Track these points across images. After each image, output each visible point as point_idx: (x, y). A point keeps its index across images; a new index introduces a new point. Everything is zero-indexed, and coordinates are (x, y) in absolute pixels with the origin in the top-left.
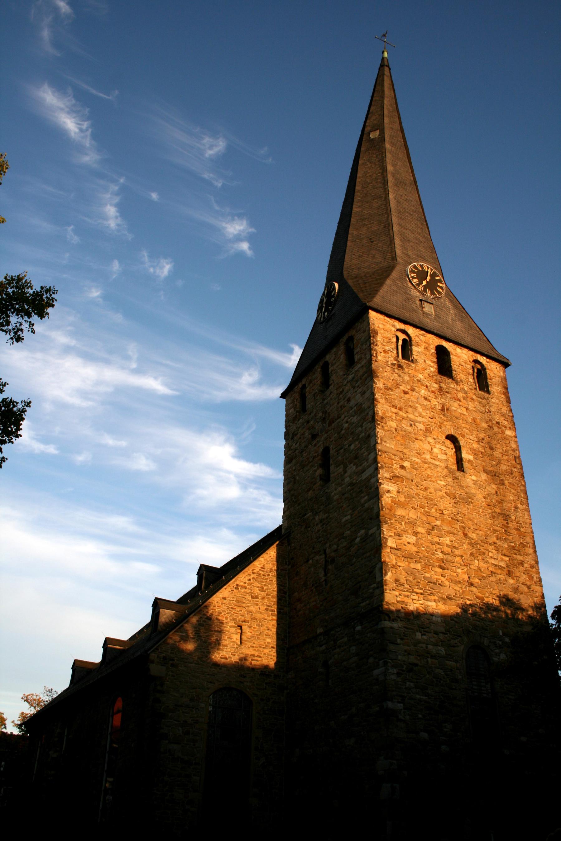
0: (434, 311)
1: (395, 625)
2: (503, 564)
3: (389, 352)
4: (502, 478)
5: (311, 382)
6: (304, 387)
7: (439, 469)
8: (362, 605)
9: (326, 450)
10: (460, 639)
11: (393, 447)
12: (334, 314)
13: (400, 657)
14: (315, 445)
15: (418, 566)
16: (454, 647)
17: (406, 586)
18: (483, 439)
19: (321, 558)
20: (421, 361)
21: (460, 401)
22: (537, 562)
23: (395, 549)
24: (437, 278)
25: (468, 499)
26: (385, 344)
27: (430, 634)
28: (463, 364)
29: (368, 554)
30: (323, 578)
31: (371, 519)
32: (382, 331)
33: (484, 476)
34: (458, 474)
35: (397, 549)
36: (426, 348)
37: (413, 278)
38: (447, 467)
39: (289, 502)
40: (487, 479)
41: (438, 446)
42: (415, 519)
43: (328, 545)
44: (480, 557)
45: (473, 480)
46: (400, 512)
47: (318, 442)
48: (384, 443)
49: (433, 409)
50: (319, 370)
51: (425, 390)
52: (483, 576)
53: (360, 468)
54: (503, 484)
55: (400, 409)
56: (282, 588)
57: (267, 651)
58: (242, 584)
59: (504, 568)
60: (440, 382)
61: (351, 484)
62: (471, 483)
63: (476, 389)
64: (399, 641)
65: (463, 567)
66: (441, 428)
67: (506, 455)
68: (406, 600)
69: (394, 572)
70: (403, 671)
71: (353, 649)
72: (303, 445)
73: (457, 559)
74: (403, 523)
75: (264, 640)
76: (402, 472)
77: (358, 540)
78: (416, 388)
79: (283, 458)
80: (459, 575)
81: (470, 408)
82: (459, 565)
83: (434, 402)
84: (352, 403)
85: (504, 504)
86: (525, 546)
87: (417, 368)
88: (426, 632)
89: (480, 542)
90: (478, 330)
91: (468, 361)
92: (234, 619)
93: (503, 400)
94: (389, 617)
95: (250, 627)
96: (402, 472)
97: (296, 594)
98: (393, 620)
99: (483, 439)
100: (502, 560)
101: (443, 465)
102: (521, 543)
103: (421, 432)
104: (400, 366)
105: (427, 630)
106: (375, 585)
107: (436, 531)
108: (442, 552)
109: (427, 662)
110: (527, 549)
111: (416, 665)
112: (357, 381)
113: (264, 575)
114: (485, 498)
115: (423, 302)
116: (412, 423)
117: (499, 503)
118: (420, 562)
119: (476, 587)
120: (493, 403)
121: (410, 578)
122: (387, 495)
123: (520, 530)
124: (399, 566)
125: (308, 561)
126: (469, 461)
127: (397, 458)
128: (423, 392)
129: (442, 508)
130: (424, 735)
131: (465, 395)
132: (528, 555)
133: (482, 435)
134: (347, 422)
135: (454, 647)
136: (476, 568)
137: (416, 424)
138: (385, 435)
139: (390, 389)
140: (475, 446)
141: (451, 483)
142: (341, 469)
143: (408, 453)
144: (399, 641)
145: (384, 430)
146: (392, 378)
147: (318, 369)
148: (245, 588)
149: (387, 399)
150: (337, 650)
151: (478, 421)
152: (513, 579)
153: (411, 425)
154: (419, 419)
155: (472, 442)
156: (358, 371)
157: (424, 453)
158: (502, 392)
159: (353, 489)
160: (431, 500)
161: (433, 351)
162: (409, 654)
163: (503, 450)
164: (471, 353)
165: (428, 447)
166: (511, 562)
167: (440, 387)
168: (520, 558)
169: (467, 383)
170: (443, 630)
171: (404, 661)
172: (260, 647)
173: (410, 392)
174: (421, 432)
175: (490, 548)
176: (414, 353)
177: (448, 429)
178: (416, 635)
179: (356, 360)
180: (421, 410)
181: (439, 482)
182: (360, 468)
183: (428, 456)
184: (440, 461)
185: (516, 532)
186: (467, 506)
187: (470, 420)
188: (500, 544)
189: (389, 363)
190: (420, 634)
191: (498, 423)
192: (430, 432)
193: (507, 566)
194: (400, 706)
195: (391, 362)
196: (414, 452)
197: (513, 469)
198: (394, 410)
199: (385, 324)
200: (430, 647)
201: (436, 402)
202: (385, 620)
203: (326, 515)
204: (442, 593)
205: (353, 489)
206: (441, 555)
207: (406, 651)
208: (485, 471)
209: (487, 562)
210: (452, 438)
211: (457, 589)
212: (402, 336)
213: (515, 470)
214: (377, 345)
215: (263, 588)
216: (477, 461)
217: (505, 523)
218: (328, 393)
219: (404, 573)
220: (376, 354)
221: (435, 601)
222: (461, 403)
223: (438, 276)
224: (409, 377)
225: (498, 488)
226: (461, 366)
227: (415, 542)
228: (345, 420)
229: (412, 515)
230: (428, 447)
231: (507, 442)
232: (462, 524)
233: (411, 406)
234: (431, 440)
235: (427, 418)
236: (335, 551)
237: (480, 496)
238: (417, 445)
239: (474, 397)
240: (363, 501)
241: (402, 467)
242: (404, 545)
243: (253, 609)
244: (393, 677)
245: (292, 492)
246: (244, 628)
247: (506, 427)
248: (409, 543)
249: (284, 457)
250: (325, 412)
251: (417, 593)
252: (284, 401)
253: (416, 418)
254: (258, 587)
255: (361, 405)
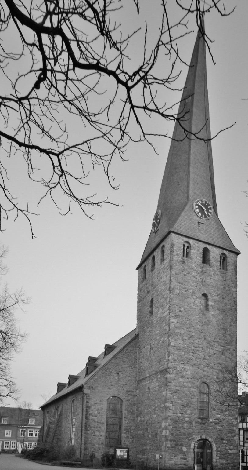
0: (205, 228)
1: (171, 376)
2: (220, 350)
3: (179, 255)
4: (226, 312)
5: (148, 264)
6: (145, 266)
7: (197, 311)
8: (161, 367)
9: (152, 300)
10: (197, 380)
11: (177, 302)
12: (158, 230)
13: (172, 388)
14: (149, 297)
15: (183, 353)
16: (195, 383)
17: (177, 361)
18: (220, 294)
19: (149, 347)
20: (194, 258)
21: (211, 276)
22: (236, 348)
23: (174, 346)
24: (209, 207)
25: (209, 323)
26: (178, 251)
27: (185, 379)
28: (216, 256)
29: (164, 348)
30: (149, 355)
31: (166, 334)
32: (177, 244)
33: (218, 312)
34: (205, 312)
35: (175, 346)
36: (198, 250)
37: (196, 209)
38: (200, 310)
39: (139, 321)
40: (219, 313)
41: (198, 300)
42: (184, 334)
43: (151, 342)
44: (211, 348)
45: (212, 314)
46: (177, 331)
47: (149, 295)
48: (173, 301)
49: (197, 282)
50: (151, 259)
51: (195, 272)
52: (211, 356)
53: (163, 311)
54: (226, 315)
55: (182, 284)
56: (135, 357)
57: (129, 382)
58: (119, 357)
59: (221, 351)
60: (202, 268)
61: (160, 317)
62: (211, 316)
63: (221, 268)
64: (172, 382)
65: (202, 352)
66: (200, 291)
67: (230, 301)
68: (177, 366)
69: (172, 355)
70: (173, 392)
71: (157, 384)
72: (144, 295)
73: (200, 349)
74: (178, 336)
75: (128, 378)
76: (180, 313)
77: (161, 342)
78: (190, 272)
79: (137, 300)
80: (200, 355)
81: (216, 279)
82: (201, 351)
83: (199, 278)
84: (162, 280)
85: (225, 324)
86: (232, 342)
87: (192, 261)
88: (184, 378)
89: (211, 341)
90: (227, 236)
91: (218, 254)
92: (116, 371)
93: (233, 273)
94: (169, 373)
95: (122, 374)
96: (180, 313)
97: (140, 360)
98: (171, 374)
99: (220, 294)
100: (220, 348)
101: (199, 308)
102: (230, 341)
103: (190, 294)
104: (184, 262)
105: (184, 377)
106: (165, 361)
107: (192, 338)
108: (194, 346)
109: (183, 389)
110: (232, 343)
111: (179, 390)
112: (165, 269)
113: (128, 353)
114: (216, 322)
115: (199, 223)
116: (187, 290)
117: (223, 323)
118: (184, 351)
119: (207, 360)
120: (228, 275)
121: (179, 358)
122: (172, 324)
123: (231, 335)
124: (175, 353)
125: (144, 347)
126: (212, 306)
127: (178, 307)
128: (193, 274)
129: (196, 328)
130: (180, 415)
131: (214, 273)
132: (232, 345)
133: (219, 292)
134: (160, 289)
135: (195, 383)
136: (208, 352)
137: (189, 290)
138: (173, 297)
139: (178, 274)
140: (216, 298)
141: (201, 316)
142: (157, 310)
143: (183, 305)
144: (172, 382)
145: (173, 295)
146: (179, 269)
147: (151, 258)
148: (120, 358)
149: (176, 279)
150: (152, 384)
151: (219, 285)
152: (224, 356)
153: (186, 291)
154: (191, 287)
155: (214, 296)
156: (165, 264)
157: (191, 304)
158: (234, 269)
159: (160, 320)
160: (191, 325)
161: (202, 251)
162: (176, 386)
163: (229, 298)
164: (221, 249)
165: (193, 300)
166: (224, 349)
167: (202, 270)
168: (228, 347)
169: (216, 266)
170: (191, 377)
171: (174, 389)
172: (126, 381)
173: (187, 274)
174: (190, 294)
175: (216, 343)
176: (192, 254)
177: (204, 291)
178: (179, 379)
179: (165, 258)
180: (192, 283)
181: (196, 316)
182: (163, 311)
183: (192, 305)
184: (198, 306)
185: (228, 336)
186: (207, 326)
187: (215, 285)
188: (221, 341)
189: (179, 261)
190: (181, 379)
191: (229, 285)
192: (195, 294)
193: (222, 351)
194: (171, 405)
195: (180, 260)
196: (186, 304)
197: (232, 307)
198: (179, 284)
199: (179, 239)
200: (185, 383)
201: (199, 279)
202: (168, 374)
203: (151, 329)
204: (192, 363)
205: (160, 320)
206: (193, 348)
207: (175, 385)
208: (218, 309)
209: (213, 350)
210: (205, 295)
211: (199, 361)
212: (186, 245)
213: (234, 308)
214: (173, 252)
215: (127, 358)
216: (216, 305)
217: (224, 332)
218: (154, 272)
219: (177, 356)
220: (173, 257)
221: (189, 366)
222: (212, 277)
223: (210, 206)
224: (188, 267)
225: (223, 317)
226: (214, 258)
227: (182, 343)
228: (159, 288)
229: (183, 331)
230: (193, 300)
231: (232, 294)
232: (204, 334)
233: (187, 282)
234: (194, 297)
235: (194, 286)
236: (154, 345)
237: (215, 321)
238: (188, 300)
239: (219, 273)
240: (163, 325)
241: (180, 311)
242: (178, 344)
243: (123, 366)
244: (169, 395)
245: (140, 316)
246: (120, 374)
247: (232, 287)
248: (180, 344)
249: (137, 299)
250: (152, 281)
251: (181, 363)
252: (137, 271)
253: (189, 287)
254: (125, 358)
255: (165, 281)
